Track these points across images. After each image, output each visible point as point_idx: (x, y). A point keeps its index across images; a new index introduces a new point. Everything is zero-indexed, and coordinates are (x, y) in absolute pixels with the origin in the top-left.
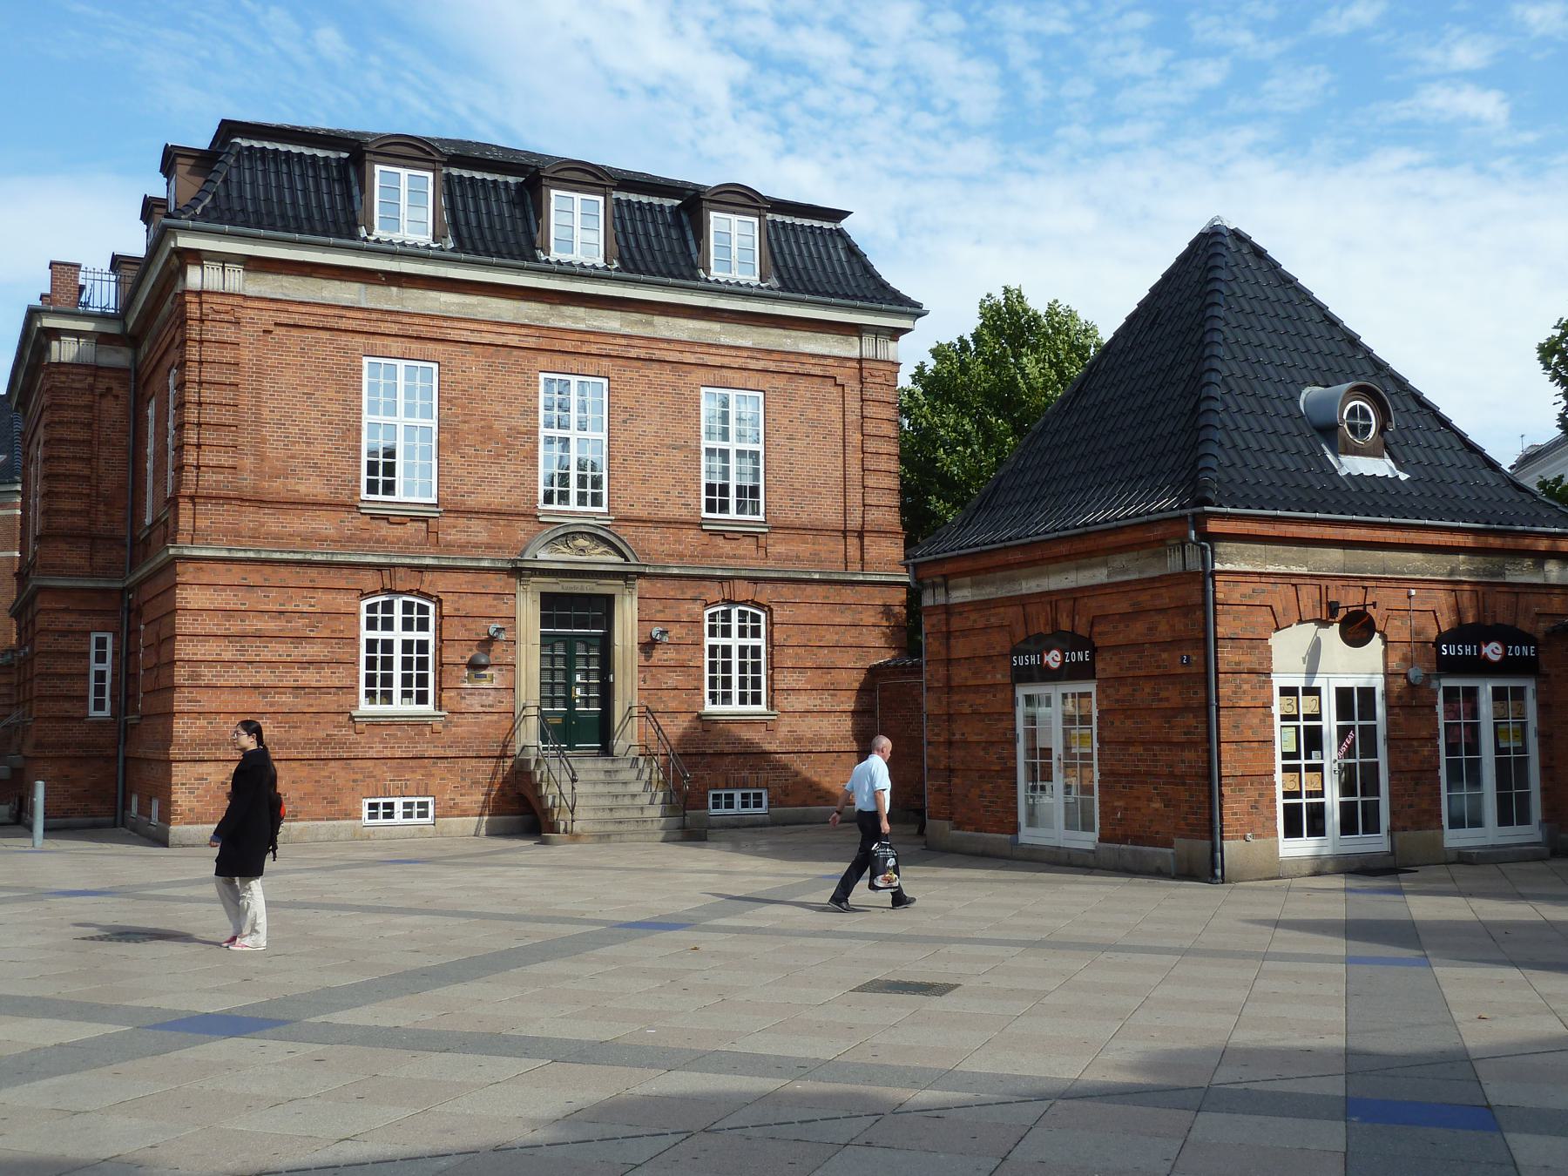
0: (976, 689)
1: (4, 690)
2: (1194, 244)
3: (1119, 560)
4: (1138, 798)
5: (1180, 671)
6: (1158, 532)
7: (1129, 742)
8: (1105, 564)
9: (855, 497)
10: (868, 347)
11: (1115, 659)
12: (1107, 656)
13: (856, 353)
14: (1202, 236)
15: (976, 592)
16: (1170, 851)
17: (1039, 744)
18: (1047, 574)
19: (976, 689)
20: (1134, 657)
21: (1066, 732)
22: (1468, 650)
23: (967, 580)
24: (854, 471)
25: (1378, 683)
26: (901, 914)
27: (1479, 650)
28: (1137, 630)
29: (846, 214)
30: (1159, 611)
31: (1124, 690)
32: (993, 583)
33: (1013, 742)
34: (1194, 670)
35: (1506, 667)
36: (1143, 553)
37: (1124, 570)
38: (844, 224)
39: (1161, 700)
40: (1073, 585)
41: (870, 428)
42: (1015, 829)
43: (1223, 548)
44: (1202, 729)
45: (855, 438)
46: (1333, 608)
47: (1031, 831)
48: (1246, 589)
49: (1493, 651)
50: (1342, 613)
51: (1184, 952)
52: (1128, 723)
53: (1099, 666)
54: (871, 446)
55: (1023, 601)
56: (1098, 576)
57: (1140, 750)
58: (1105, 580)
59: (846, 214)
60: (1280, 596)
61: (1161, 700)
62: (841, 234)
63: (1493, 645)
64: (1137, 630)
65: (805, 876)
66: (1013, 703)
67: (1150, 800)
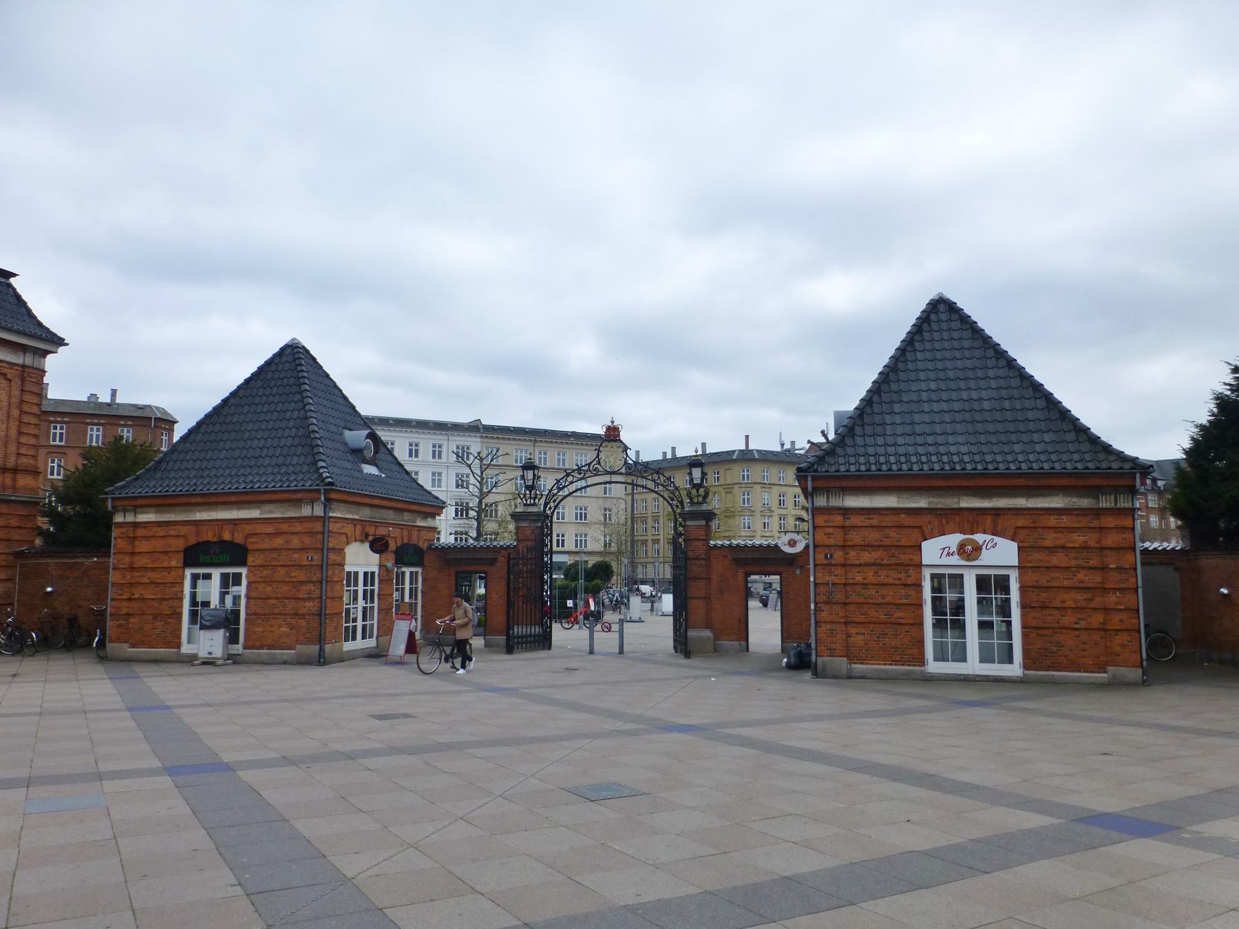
0: (154, 569)
1: (3, 576)
2: (283, 350)
3: (268, 507)
6: (299, 496)
9: (12, 448)
10: (28, 360)
13: (20, 361)
14: (287, 347)
17: (199, 599)
19: (154, 569)
24: (13, 433)
25: (376, 569)
26: (591, 657)
28: (278, 542)
29: (14, 275)
30: (293, 533)
31: (266, 572)
33: (181, 599)
37: (272, 512)
38: (12, 280)
41: (26, 408)
42: (179, 646)
43: (334, 505)
44: (318, 592)
45: (16, 413)
46: (367, 536)
47: (190, 646)
48: (339, 525)
50: (371, 538)
52: (268, 589)
54: (26, 419)
55: (197, 523)
56: (255, 513)
57: (274, 602)
59: (14, 275)
60: (349, 529)
62: (10, 286)
64: (278, 542)
66: (183, 577)
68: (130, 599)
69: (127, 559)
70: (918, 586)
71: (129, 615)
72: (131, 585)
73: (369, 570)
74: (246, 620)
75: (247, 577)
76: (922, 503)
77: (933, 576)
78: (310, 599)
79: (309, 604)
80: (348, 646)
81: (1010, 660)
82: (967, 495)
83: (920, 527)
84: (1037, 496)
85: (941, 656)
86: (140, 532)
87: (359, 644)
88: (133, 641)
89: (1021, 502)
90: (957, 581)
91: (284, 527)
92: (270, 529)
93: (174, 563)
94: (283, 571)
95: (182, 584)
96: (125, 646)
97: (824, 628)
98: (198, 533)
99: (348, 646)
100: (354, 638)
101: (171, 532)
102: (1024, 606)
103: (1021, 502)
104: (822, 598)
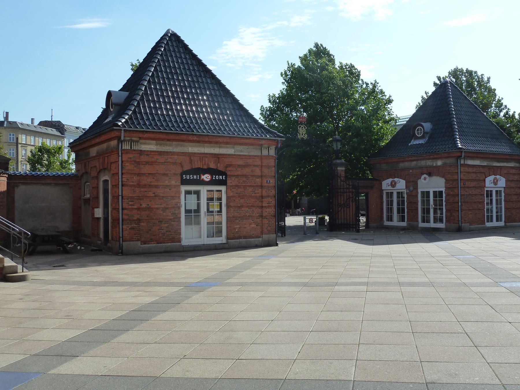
3: (239, 148)
4: (245, 224)
5: (267, 185)
7: (242, 206)
8: (233, 148)
11: (237, 179)
12: (233, 178)
15: (158, 147)
16: (261, 239)
18: (204, 147)
20: (245, 180)
21: (208, 204)
22: (195, 177)
23: (154, 142)
25: (443, 190)
27: (200, 177)
30: (255, 166)
31: (240, 190)
32: (171, 146)
33: (179, 208)
34: (271, 185)
35: (212, 182)
36: (250, 147)
37: (241, 151)
39: (255, 193)
40: (217, 152)
49: (206, 177)
51: (332, 257)
53: (229, 181)
55: (191, 155)
58: (233, 153)
61: (255, 193)
63: (206, 175)
65: (279, 257)
66: (179, 192)
67: (250, 224)
68: (138, 209)
69: (135, 178)
70: (417, 196)
71: (139, 220)
72: (139, 198)
73: (441, 190)
74: (112, 222)
75: (504, 192)
76: (485, 164)
77: (386, 193)
78: (269, 207)
79: (269, 210)
80: (488, 224)
81: (501, 221)
82: (470, 160)
83: (484, 173)
84: (510, 162)
85: (423, 221)
86: (144, 158)
87: (495, 223)
88: (143, 239)
89: (505, 164)
90: (392, 193)
91: (250, 161)
92: (241, 162)
93: (173, 182)
94: (251, 189)
95: (179, 197)
96: (139, 243)
97: (464, 212)
98: (191, 161)
99: (488, 224)
100: (492, 221)
101: (169, 160)
102: (505, 201)
103: (505, 164)
104: (463, 200)
